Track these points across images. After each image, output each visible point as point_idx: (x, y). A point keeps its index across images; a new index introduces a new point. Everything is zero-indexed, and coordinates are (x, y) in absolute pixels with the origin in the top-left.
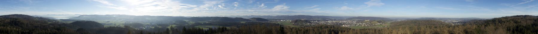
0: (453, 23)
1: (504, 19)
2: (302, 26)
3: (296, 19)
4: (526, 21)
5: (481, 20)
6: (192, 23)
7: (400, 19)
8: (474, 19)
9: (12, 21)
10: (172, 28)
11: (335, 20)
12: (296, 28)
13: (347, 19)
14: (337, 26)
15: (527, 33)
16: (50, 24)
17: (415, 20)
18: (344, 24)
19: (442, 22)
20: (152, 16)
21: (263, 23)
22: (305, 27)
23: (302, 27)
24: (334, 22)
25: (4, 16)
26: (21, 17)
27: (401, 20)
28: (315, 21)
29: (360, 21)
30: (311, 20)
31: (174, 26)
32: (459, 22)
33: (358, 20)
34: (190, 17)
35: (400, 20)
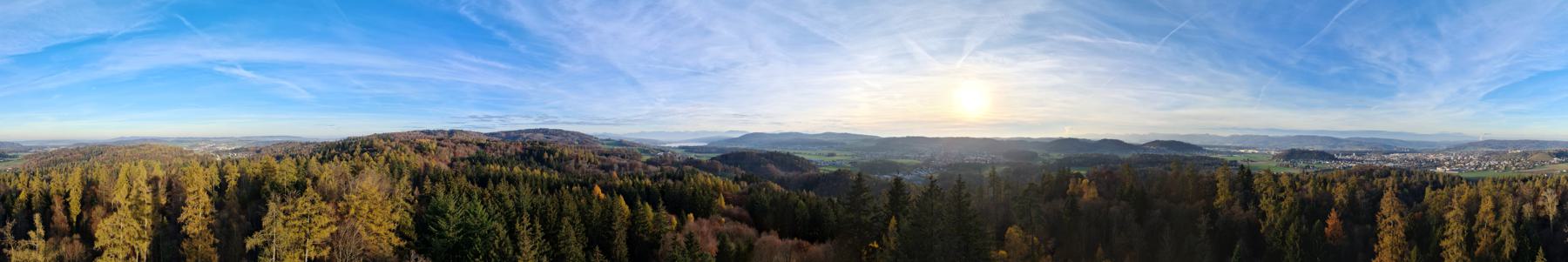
0: (218, 152)
1: (382, 141)
2: (1308, 170)
3: (1289, 148)
4: (455, 148)
5: (307, 144)
6: (1056, 156)
7: (51, 144)
8: (286, 139)
9: (531, 150)
10: (994, 176)
11: (1412, 151)
12: (1290, 175)
13: (1448, 149)
14: (1418, 170)
15: (487, 257)
16: (649, 162)
17: (99, 146)
18: (1439, 164)
19: (181, 151)
20: (957, 138)
21: (1186, 159)
22: (1317, 172)
23: (1307, 173)
24: (1411, 156)
25: (504, 135)
26: (557, 138)
27: (55, 147)
28: (1350, 153)
29: (1494, 153)
30: (1335, 152)
31: (999, 170)
32: (236, 151)
33: (1485, 150)
34: (1048, 141)
35: (52, 147)
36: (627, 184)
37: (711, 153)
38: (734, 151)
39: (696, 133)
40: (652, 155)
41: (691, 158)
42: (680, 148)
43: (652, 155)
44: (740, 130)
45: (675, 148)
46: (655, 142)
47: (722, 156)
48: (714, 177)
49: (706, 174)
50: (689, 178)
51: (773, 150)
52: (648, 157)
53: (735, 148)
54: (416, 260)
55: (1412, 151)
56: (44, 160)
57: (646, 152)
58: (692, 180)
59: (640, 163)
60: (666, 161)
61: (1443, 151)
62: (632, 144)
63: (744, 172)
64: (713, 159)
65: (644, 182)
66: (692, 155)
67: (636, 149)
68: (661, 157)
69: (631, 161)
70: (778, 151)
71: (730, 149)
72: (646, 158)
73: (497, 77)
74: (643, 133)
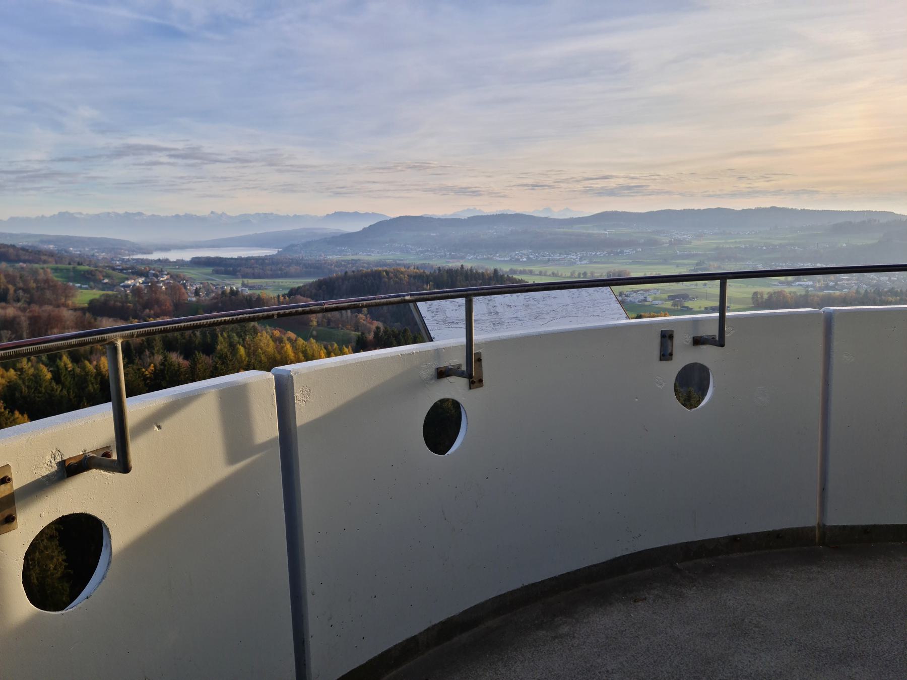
16: (97, 309)
36: (37, 378)
37: (286, 275)
38: (350, 269)
39: (244, 220)
40: (111, 286)
41: (233, 293)
42: (197, 262)
43: (105, 287)
44: (362, 210)
45: (180, 263)
46: (114, 246)
47: (320, 285)
48: (301, 341)
49: (277, 333)
50: (232, 346)
51: (455, 264)
52: (96, 294)
53: (354, 262)
54: (3, 377)
55: (556, 264)
56: (572, 260)
57: (88, 278)
58: (242, 350)
59: (67, 314)
60: (158, 302)
61: (554, 260)
62: (33, 254)
63: (377, 324)
64: (293, 293)
65: (90, 367)
66: (236, 284)
67: (46, 270)
68: (136, 291)
69: (35, 308)
70: (468, 265)
71: (338, 264)
72: (84, 296)
73: (434, 345)
74: (64, 218)
